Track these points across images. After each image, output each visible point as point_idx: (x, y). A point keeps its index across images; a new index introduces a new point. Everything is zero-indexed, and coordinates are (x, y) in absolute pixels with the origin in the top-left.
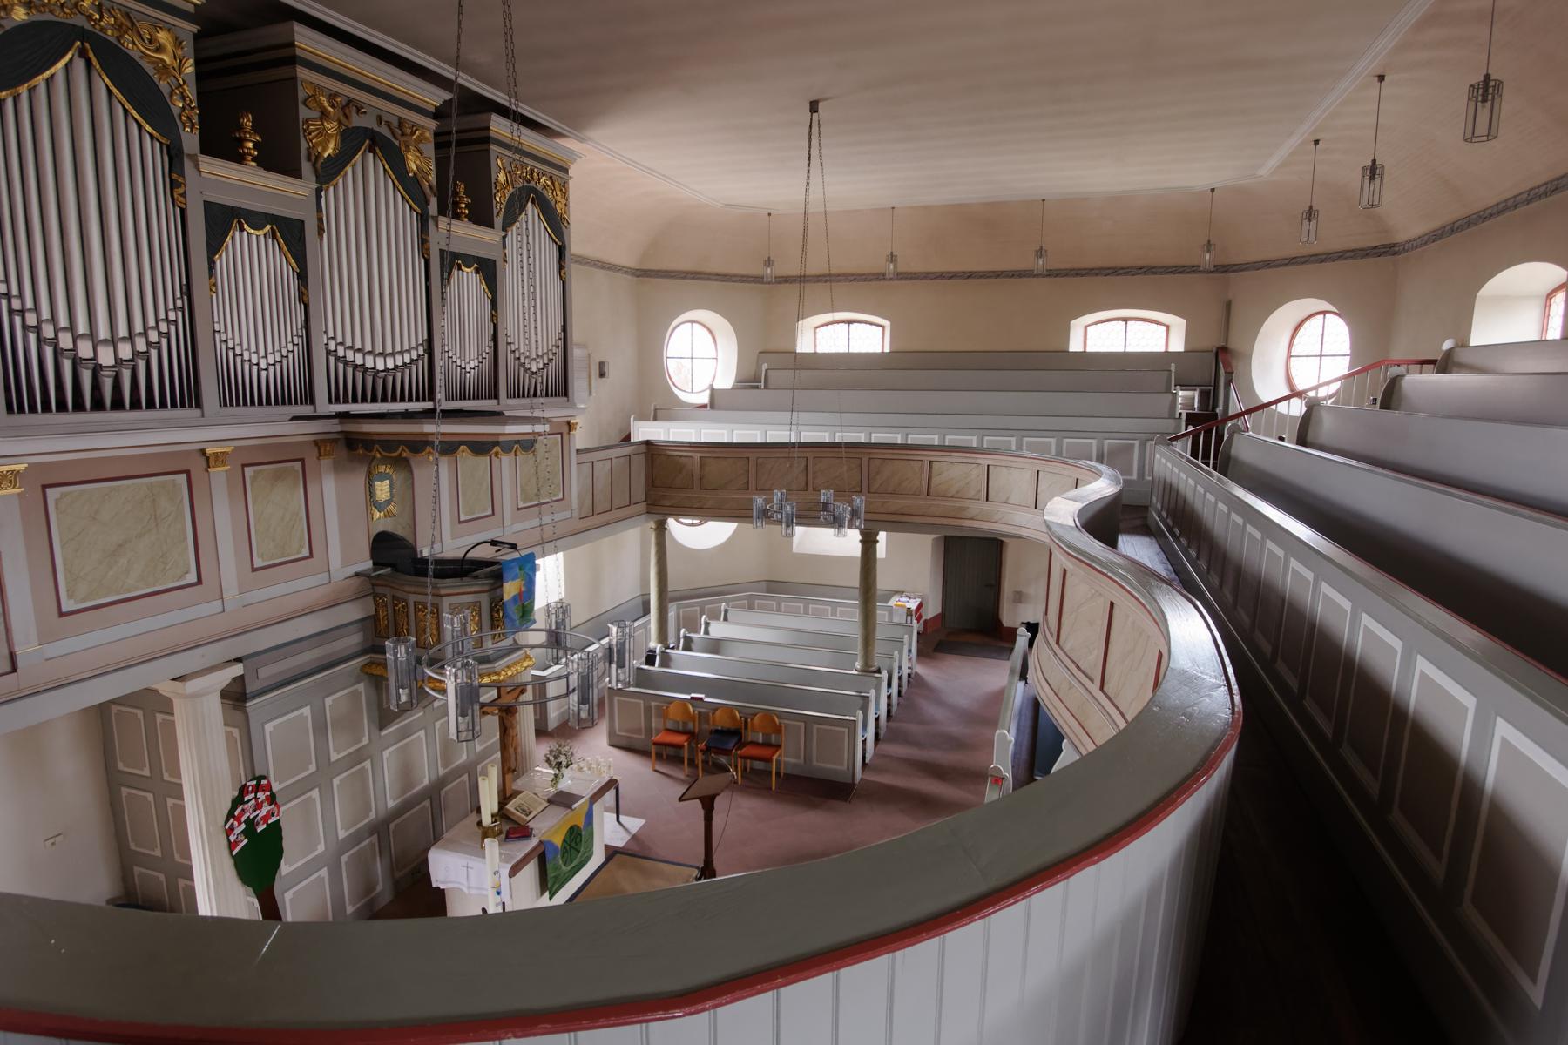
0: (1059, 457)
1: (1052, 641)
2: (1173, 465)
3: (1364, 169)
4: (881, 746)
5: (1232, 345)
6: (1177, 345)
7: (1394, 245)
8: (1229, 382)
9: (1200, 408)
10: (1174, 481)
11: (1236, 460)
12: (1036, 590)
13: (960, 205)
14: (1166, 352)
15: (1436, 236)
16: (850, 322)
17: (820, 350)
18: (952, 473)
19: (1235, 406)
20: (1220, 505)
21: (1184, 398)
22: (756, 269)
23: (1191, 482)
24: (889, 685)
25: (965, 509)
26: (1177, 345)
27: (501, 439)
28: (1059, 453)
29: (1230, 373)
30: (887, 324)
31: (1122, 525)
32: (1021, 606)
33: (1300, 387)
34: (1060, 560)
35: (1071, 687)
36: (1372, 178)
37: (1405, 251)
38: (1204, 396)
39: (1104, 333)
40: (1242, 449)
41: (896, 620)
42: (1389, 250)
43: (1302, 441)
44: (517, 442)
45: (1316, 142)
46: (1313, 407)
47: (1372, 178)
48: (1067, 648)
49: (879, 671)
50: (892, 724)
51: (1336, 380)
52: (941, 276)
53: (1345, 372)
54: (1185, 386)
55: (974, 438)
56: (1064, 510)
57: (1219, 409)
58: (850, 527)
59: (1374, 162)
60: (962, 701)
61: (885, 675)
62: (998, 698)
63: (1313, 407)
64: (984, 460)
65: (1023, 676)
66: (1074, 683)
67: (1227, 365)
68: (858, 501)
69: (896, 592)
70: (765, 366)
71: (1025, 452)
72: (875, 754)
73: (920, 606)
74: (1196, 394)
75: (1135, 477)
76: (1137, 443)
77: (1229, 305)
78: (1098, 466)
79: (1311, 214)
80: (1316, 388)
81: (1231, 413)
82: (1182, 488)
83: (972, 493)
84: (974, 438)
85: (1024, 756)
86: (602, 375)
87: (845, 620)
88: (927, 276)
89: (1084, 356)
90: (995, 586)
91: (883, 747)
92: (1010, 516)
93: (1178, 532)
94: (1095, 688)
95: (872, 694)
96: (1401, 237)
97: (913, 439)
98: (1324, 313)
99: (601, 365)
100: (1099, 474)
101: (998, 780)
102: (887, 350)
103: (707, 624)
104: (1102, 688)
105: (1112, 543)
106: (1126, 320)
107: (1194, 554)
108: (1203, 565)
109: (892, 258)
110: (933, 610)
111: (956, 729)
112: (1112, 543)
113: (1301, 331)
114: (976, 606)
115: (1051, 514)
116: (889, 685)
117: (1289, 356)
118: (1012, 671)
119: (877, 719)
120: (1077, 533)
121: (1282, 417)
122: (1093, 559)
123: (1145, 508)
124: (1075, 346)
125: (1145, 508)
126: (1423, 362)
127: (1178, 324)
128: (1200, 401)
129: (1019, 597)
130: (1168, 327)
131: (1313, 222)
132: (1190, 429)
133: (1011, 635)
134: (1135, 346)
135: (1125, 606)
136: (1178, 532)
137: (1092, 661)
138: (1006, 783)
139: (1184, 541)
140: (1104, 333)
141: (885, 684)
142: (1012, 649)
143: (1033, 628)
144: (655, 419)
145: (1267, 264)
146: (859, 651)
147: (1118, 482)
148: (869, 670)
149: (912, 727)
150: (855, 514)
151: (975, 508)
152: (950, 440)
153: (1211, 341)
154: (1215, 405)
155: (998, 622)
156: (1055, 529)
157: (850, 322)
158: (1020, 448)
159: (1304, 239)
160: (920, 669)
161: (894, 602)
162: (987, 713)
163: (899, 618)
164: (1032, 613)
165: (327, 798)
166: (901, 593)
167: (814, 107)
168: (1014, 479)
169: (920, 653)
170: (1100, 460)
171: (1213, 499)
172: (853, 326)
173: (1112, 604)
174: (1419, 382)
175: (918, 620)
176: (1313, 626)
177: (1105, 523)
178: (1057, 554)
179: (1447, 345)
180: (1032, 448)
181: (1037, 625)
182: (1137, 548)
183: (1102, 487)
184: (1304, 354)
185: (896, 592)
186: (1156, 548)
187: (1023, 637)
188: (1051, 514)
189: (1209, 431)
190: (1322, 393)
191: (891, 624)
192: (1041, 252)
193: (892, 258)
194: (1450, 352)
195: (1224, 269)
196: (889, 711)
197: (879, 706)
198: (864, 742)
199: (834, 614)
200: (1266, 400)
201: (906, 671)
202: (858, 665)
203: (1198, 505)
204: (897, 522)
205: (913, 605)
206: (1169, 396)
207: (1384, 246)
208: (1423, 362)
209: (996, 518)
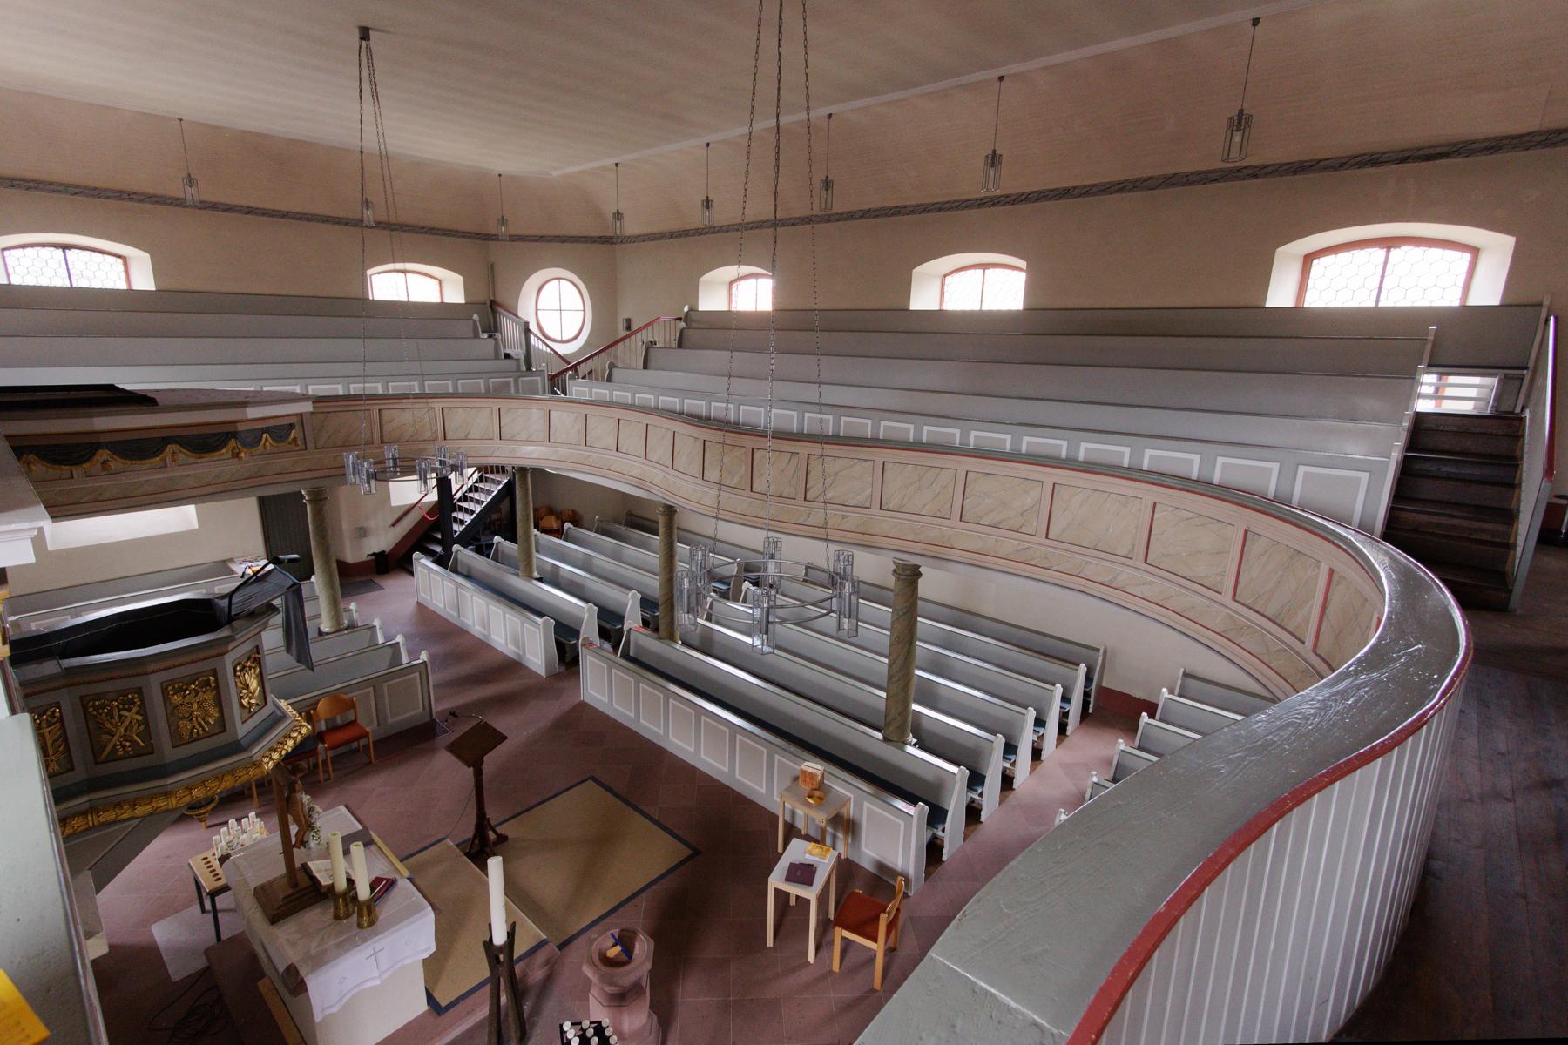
13: (265, 136)
17: (413, 299)
22: (175, 189)
27: (241, 427)
32: (366, 541)
39: (393, 284)
44: (264, 430)
64: (438, 404)
83: (428, 435)
106: (65, 247)
109: (190, 181)
127: (142, 261)
130: (440, 282)
140: (393, 284)
153: (482, 296)
165: (930, 697)
167: (365, 34)
172: (71, 254)
179: (686, 309)
184: (557, 309)
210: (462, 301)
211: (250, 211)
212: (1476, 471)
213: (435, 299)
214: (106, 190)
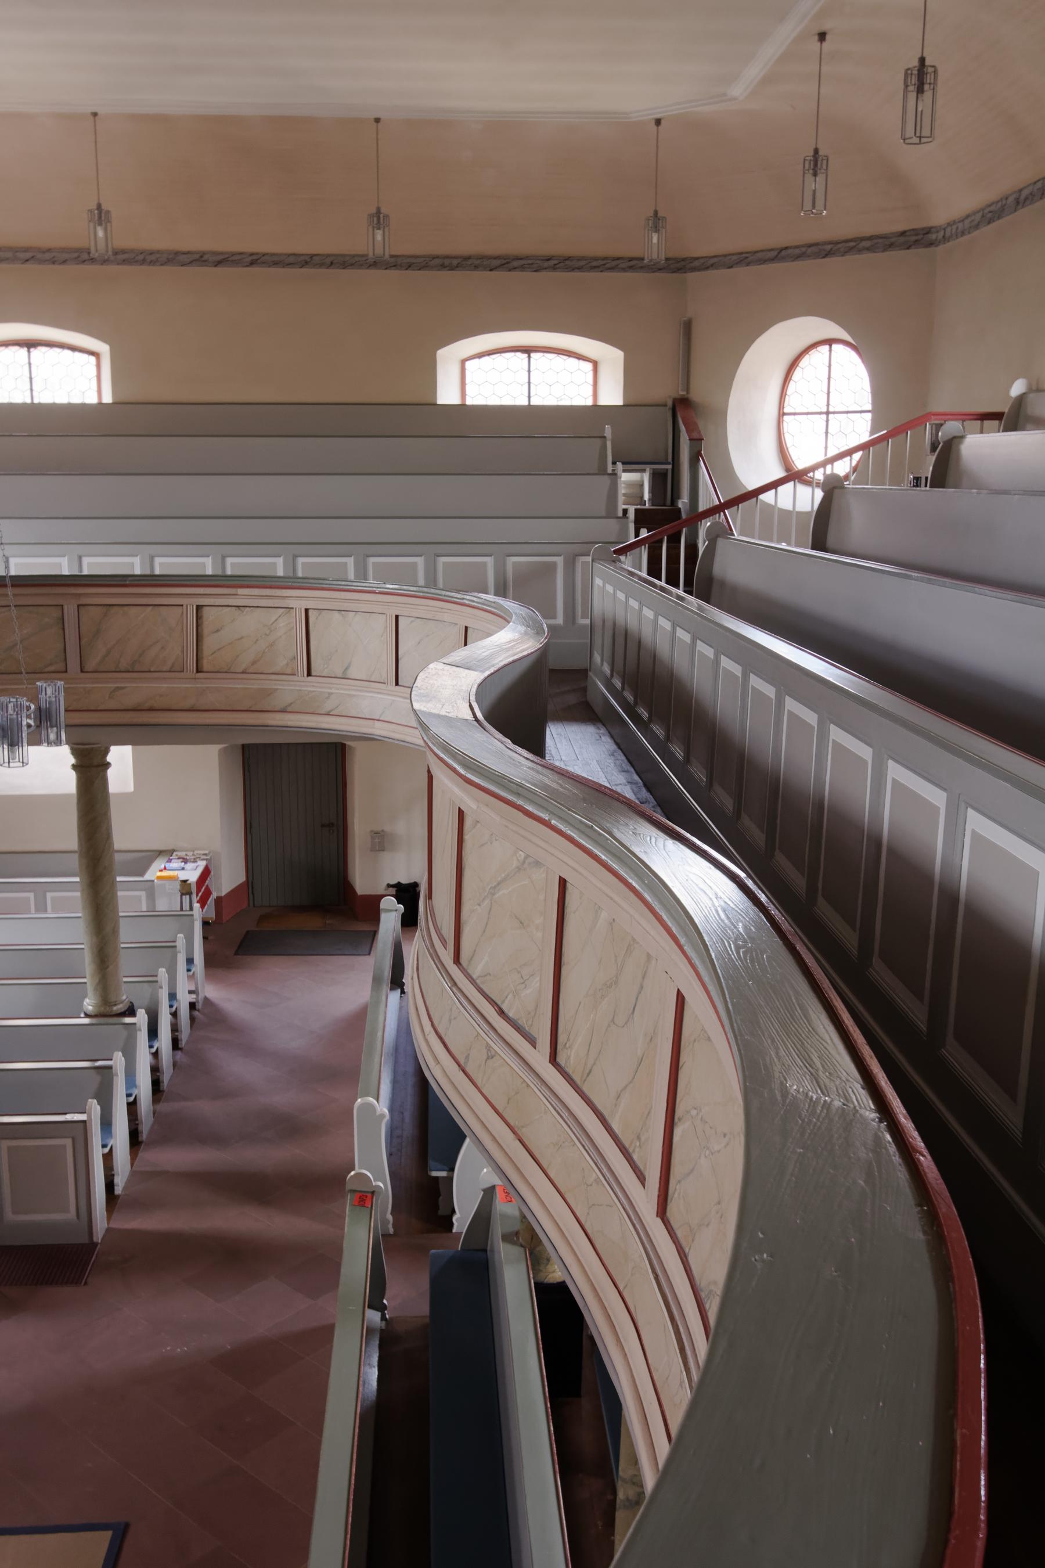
0: (432, 589)
1: (447, 956)
2: (625, 596)
3: (907, 73)
4: (144, 1155)
5: (695, 395)
6: (612, 395)
7: (928, 231)
8: (696, 457)
9: (652, 500)
10: (633, 624)
11: (723, 584)
12: (409, 827)
14: (595, 407)
15: (992, 214)
16: (30, 344)
17: (44, 397)
18: (245, 627)
19: (708, 497)
20: (726, 663)
21: (630, 485)
23: (665, 624)
24: (153, 1033)
25: (268, 693)
26: (612, 395)
28: (432, 581)
29: (696, 441)
30: (103, 348)
31: (550, 707)
32: (386, 857)
33: (800, 464)
34: (450, 791)
35: (491, 1056)
36: (920, 90)
37: (945, 239)
38: (658, 479)
40: (730, 566)
41: (163, 905)
42: (920, 238)
43: (819, 543)
45: (822, 36)
46: (833, 488)
47: (920, 90)
48: (476, 972)
49: (131, 1012)
50: (164, 1107)
51: (849, 453)
52: (200, 259)
53: (865, 437)
54: (631, 463)
55: (280, 561)
56: (449, 689)
57: (683, 503)
58: (35, 741)
59: (922, 60)
60: (291, 1041)
61: (141, 1018)
62: (357, 1024)
63: (833, 488)
64: (299, 600)
65: (397, 982)
66: (497, 1047)
67: (691, 427)
68: (51, 691)
69: (160, 853)
71: (372, 583)
72: (135, 1175)
73: (206, 873)
74: (646, 478)
75: (560, 620)
76: (560, 561)
77: (688, 327)
78: (500, 601)
79: (816, 163)
80: (823, 464)
81: (702, 507)
82: (647, 633)
83: (281, 663)
84: (280, 561)
85: (409, 1128)
87: (57, 920)
88: (174, 258)
89: (462, 411)
90: (338, 826)
91: (151, 1157)
92: (351, 704)
93: (645, 715)
94: (539, 1058)
95: (118, 1061)
96: (939, 217)
97: (164, 564)
98: (830, 342)
100: (505, 618)
101: (365, 1198)
102: (108, 398)
104: (553, 1059)
105: (533, 743)
106: (528, 350)
107: (679, 753)
108: (700, 774)
109: (101, 215)
110: (230, 877)
111: (285, 1099)
112: (533, 743)
113: (797, 374)
114: (306, 871)
115: (428, 697)
116: (153, 1033)
117: (781, 414)
118: (377, 981)
119: (132, 1106)
120: (479, 735)
121: (769, 508)
122: (518, 789)
123: (583, 674)
124: (447, 395)
125: (583, 674)
126: (985, 417)
127: (612, 357)
128: (652, 490)
129: (381, 841)
130: (595, 364)
131: (821, 178)
132: (644, 533)
133: (371, 908)
134: (545, 397)
135: (589, 884)
136: (645, 715)
137: (530, 998)
138: (377, 1201)
139: (659, 731)
141: (143, 1036)
142: (375, 933)
143: (407, 894)
145: (744, 259)
146: (89, 979)
147: (539, 632)
148: (112, 1012)
149: (204, 1108)
150: (44, 717)
151: (293, 688)
152: (234, 565)
153: (665, 390)
154: (676, 495)
155: (346, 886)
156: (439, 729)
157: (30, 344)
158: (362, 574)
159: (808, 205)
160: (212, 992)
161: (155, 872)
162: (336, 1063)
163: (168, 902)
164: (405, 867)
166: (167, 853)
168: (354, 632)
169: (210, 961)
170: (501, 591)
171: (709, 652)
172: (38, 353)
173: (563, 883)
174: (982, 447)
175: (203, 902)
176: (950, 898)
177: (521, 709)
178: (444, 781)
179: (1017, 388)
180: (386, 574)
181: (415, 886)
182: (579, 749)
183: (509, 641)
184: (804, 408)
185: (160, 853)
186: (608, 744)
187: (391, 913)
188: (428, 697)
189: (673, 537)
190: (842, 468)
191: (153, 915)
192: (378, 219)
193: (101, 215)
194: (1021, 399)
195: (679, 265)
196: (156, 1083)
197: (134, 1072)
198: (108, 1158)
199: (41, 907)
200: (751, 483)
201: (184, 999)
202: (89, 1004)
203: (680, 664)
204: (145, 727)
205: (192, 874)
206: (606, 480)
207: (915, 231)
208: (985, 417)
209: (328, 706)
210: (620, 402)
211: (255, 260)
212: (742, 875)
213: (584, 399)
214: (63, 250)
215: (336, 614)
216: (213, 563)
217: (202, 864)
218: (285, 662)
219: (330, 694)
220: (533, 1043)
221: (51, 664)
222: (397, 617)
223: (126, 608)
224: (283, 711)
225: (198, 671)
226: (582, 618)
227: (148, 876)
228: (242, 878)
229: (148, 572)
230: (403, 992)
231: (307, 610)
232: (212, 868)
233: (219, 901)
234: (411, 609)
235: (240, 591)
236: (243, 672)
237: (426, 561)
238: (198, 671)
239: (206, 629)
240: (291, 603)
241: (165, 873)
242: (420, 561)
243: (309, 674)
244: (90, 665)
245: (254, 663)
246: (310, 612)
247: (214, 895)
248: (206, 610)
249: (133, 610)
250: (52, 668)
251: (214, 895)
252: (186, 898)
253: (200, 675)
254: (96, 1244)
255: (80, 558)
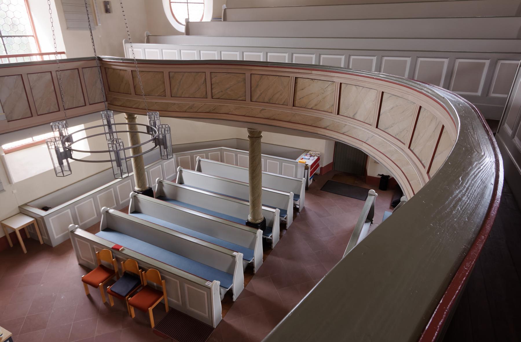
4: (270, 257)
25: (320, 119)
55: (314, 56)
64: (338, 78)
70: (224, 6)
83: (327, 107)
84: (314, 56)
86: (107, 11)
99: (106, 4)
103: (181, 171)
144: (148, 42)
209: (344, 130)
215: (354, 87)
216: (345, 58)
217: (316, 158)
218: (328, 107)
219: (346, 125)
220: (424, 167)
221: (240, 97)
222: (383, 93)
223: (268, 76)
224: (325, 128)
225: (293, 106)
226: (493, 93)
227: (297, 160)
228: (331, 161)
229: (241, 60)
230: (372, 223)
231: (341, 84)
232: (320, 158)
233: (321, 168)
234: (390, 89)
235: (314, 72)
236: (311, 109)
237: (377, 59)
238: (293, 106)
239: (298, 88)
240: (335, 80)
241: (302, 161)
242: (409, 60)
243: (338, 114)
244: (254, 99)
245: (316, 105)
246: (342, 85)
247: (320, 166)
248: (299, 79)
249: (271, 77)
250: (241, 99)
251: (320, 166)
252: (306, 171)
253: (294, 107)
254: (214, 328)
255: (267, 53)
